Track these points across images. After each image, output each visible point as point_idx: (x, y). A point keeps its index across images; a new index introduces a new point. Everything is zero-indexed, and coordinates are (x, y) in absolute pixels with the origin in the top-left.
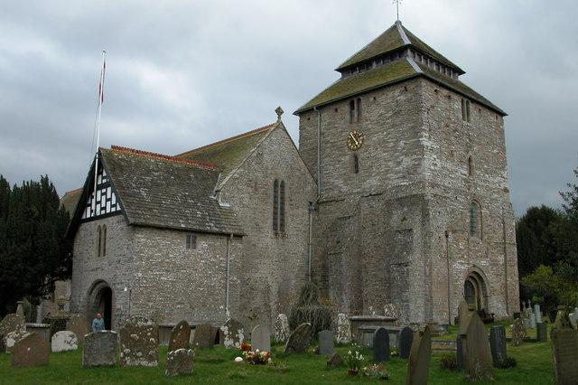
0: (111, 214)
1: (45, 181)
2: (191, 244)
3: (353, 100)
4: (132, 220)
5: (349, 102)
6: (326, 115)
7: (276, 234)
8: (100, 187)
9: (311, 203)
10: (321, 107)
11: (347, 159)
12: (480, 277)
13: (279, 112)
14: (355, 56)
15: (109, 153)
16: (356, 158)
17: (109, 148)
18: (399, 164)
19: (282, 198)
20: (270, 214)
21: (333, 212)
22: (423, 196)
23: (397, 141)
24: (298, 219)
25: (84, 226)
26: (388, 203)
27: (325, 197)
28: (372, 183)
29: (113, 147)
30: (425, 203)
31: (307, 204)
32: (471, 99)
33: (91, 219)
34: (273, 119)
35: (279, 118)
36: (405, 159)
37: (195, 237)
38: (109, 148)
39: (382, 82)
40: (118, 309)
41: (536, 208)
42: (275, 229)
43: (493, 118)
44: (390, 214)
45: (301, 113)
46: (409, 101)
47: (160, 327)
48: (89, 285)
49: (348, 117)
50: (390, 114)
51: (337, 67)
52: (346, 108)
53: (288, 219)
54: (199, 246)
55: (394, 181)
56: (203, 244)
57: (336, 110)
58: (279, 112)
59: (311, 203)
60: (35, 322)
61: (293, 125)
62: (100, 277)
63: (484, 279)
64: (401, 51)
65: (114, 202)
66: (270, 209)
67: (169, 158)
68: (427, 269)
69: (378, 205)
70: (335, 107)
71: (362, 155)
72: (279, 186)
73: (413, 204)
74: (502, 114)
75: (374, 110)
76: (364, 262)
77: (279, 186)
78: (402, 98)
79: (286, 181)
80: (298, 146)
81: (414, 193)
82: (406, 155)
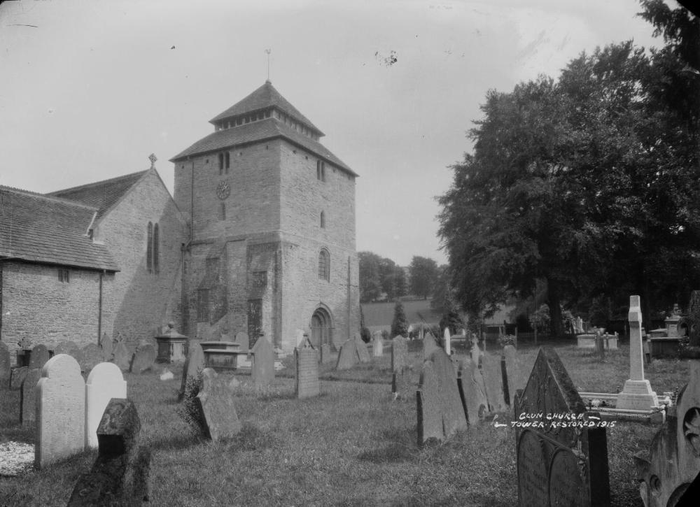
1: (444, 201)
3: (223, 155)
9: (183, 245)
12: (325, 311)
13: (153, 159)
17: (212, 129)
29: (221, 122)
32: (325, 162)
35: (152, 164)
37: (68, 272)
38: (212, 129)
39: (249, 138)
41: (394, 263)
45: (179, 160)
51: (210, 119)
57: (207, 161)
58: (153, 159)
59: (183, 245)
61: (168, 173)
63: (330, 314)
64: (267, 111)
74: (351, 175)
79: (160, 226)
80: (172, 191)
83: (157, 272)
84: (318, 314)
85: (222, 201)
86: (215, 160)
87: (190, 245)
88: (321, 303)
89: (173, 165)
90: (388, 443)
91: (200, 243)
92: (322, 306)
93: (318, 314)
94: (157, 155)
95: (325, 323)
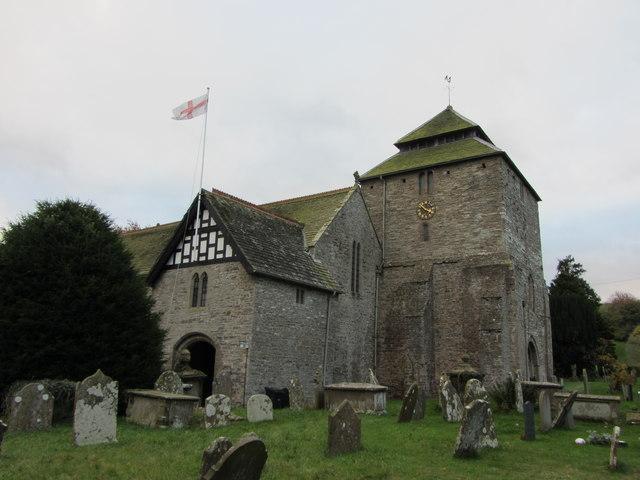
0: (216, 261)
2: (300, 299)
4: (255, 269)
6: (392, 185)
7: (353, 294)
8: (201, 231)
10: (387, 177)
11: (416, 227)
14: (413, 133)
15: (212, 197)
16: (426, 225)
18: (476, 234)
19: (358, 260)
20: (349, 275)
21: (403, 277)
22: (508, 266)
23: (474, 213)
24: (368, 278)
25: (171, 272)
26: (466, 271)
27: (389, 263)
28: (446, 251)
30: (509, 273)
31: (375, 268)
33: (182, 265)
36: (484, 231)
37: (303, 292)
40: (226, 367)
42: (353, 290)
44: (468, 283)
46: (488, 177)
47: (326, 389)
48: (179, 338)
49: (417, 188)
50: (466, 187)
51: (396, 141)
52: (415, 179)
53: (362, 281)
54: (306, 302)
55: (469, 251)
56: (309, 299)
57: (404, 181)
60: (152, 387)
62: (196, 329)
65: (220, 247)
66: (350, 268)
67: (254, 206)
68: (513, 337)
69: (454, 273)
70: (403, 178)
71: (433, 224)
72: (356, 246)
73: (495, 273)
74: (537, 199)
75: (446, 185)
76: (436, 326)
77: (356, 246)
78: (480, 174)
81: (496, 263)
82: (485, 227)
91: (393, 267)
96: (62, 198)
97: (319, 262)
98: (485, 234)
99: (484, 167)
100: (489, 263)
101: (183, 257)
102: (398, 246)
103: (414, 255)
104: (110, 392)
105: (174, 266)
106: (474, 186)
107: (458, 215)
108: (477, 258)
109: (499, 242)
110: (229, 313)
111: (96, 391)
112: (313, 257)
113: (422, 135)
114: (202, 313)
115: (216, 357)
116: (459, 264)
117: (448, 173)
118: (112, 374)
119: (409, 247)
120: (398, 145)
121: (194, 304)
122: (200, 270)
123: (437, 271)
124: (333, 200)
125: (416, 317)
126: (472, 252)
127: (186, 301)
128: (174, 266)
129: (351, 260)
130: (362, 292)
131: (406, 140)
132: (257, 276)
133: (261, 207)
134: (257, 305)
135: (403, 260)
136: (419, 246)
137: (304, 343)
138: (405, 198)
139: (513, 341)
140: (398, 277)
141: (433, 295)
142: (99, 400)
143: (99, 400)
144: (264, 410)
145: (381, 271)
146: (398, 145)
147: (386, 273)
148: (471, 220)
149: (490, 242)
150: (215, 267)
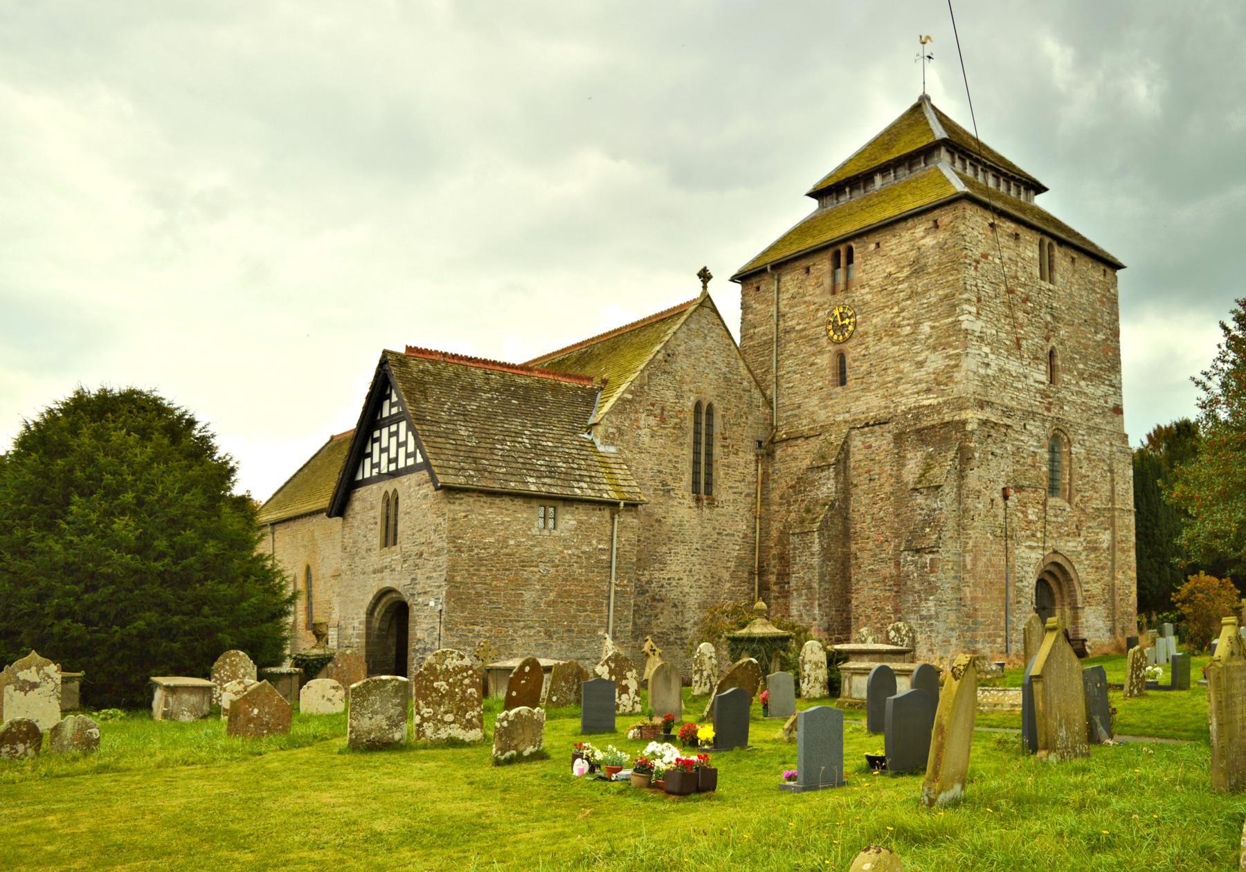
5: (830, 252)
7: (698, 500)
11: (825, 361)
17: (403, 351)
18: (920, 364)
22: (964, 423)
23: (917, 324)
24: (736, 470)
25: (361, 493)
26: (899, 438)
28: (870, 403)
29: (409, 349)
30: (967, 435)
31: (754, 445)
34: (692, 290)
35: (705, 287)
36: (932, 357)
38: (403, 351)
43: (1096, 274)
45: (744, 278)
46: (942, 247)
49: (827, 281)
51: (809, 188)
55: (909, 400)
57: (808, 270)
58: (705, 276)
59: (760, 443)
61: (728, 299)
62: (388, 583)
66: (688, 453)
68: (968, 559)
69: (882, 442)
71: (853, 352)
72: (703, 413)
78: (929, 241)
81: (947, 419)
82: (935, 349)
83: (712, 503)
84: (1047, 577)
85: (838, 347)
86: (823, 265)
87: (772, 442)
88: (1055, 552)
89: (738, 287)
90: (692, 602)
91: (791, 439)
92: (1059, 560)
93: (1047, 577)
94: (711, 270)
95: (1062, 597)
96: (17, 430)
97: (612, 449)
98: (936, 362)
99: (937, 227)
100: (935, 419)
101: (373, 466)
102: (797, 400)
103: (822, 416)
104: (49, 677)
105: (365, 482)
106: (918, 269)
107: (891, 329)
108: (918, 412)
109: (958, 376)
110: (421, 554)
111: (30, 675)
112: (598, 442)
113: (851, 172)
114: (392, 556)
115: (410, 625)
116: (891, 426)
117: (878, 245)
118: (53, 656)
119: (815, 400)
120: (816, 194)
121: (385, 544)
122: (388, 486)
123: (857, 443)
124: (650, 333)
125: (807, 533)
126: (911, 401)
127: (376, 538)
128: (365, 482)
129: (689, 439)
130: (722, 493)
131: (825, 185)
132: (450, 491)
133: (525, 367)
134: (452, 540)
135: (804, 425)
136: (829, 397)
137: (559, 595)
138: (808, 303)
139: (969, 567)
140: (795, 459)
141: (846, 490)
142: (34, 686)
143: (34, 686)
144: (330, 700)
145: (767, 449)
146: (816, 194)
147: (779, 453)
148: (913, 338)
149: (942, 379)
150: (404, 479)
